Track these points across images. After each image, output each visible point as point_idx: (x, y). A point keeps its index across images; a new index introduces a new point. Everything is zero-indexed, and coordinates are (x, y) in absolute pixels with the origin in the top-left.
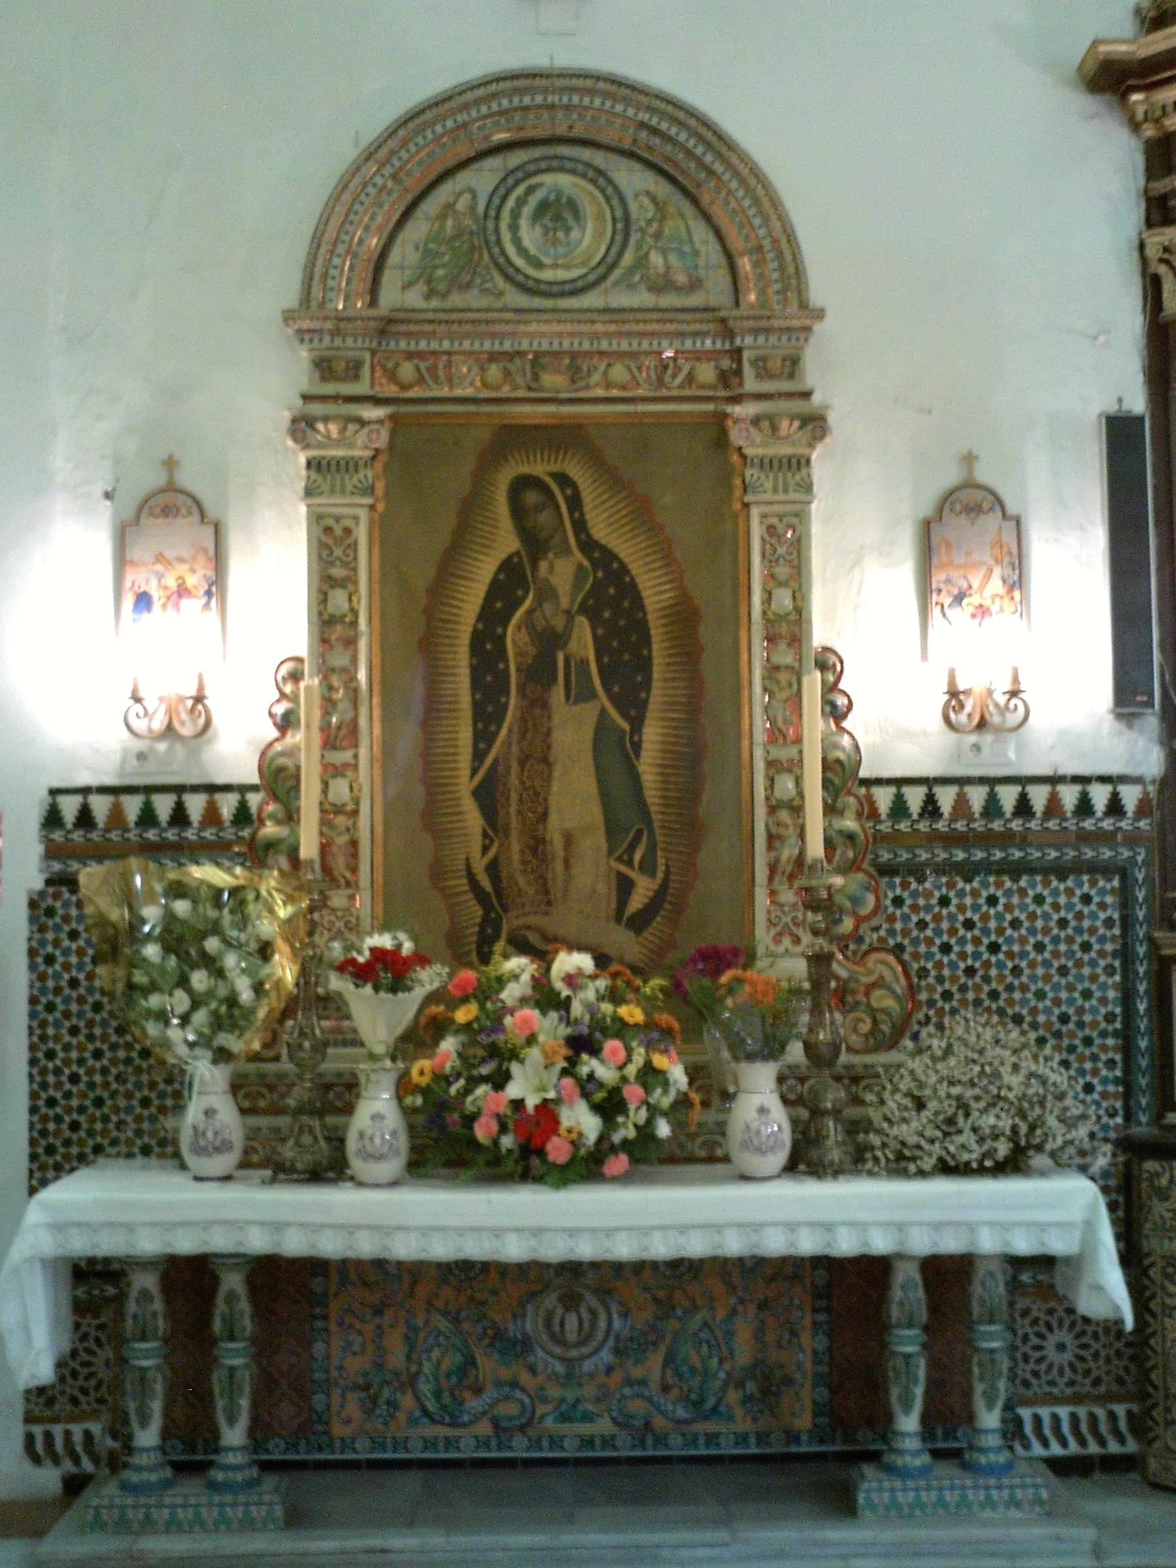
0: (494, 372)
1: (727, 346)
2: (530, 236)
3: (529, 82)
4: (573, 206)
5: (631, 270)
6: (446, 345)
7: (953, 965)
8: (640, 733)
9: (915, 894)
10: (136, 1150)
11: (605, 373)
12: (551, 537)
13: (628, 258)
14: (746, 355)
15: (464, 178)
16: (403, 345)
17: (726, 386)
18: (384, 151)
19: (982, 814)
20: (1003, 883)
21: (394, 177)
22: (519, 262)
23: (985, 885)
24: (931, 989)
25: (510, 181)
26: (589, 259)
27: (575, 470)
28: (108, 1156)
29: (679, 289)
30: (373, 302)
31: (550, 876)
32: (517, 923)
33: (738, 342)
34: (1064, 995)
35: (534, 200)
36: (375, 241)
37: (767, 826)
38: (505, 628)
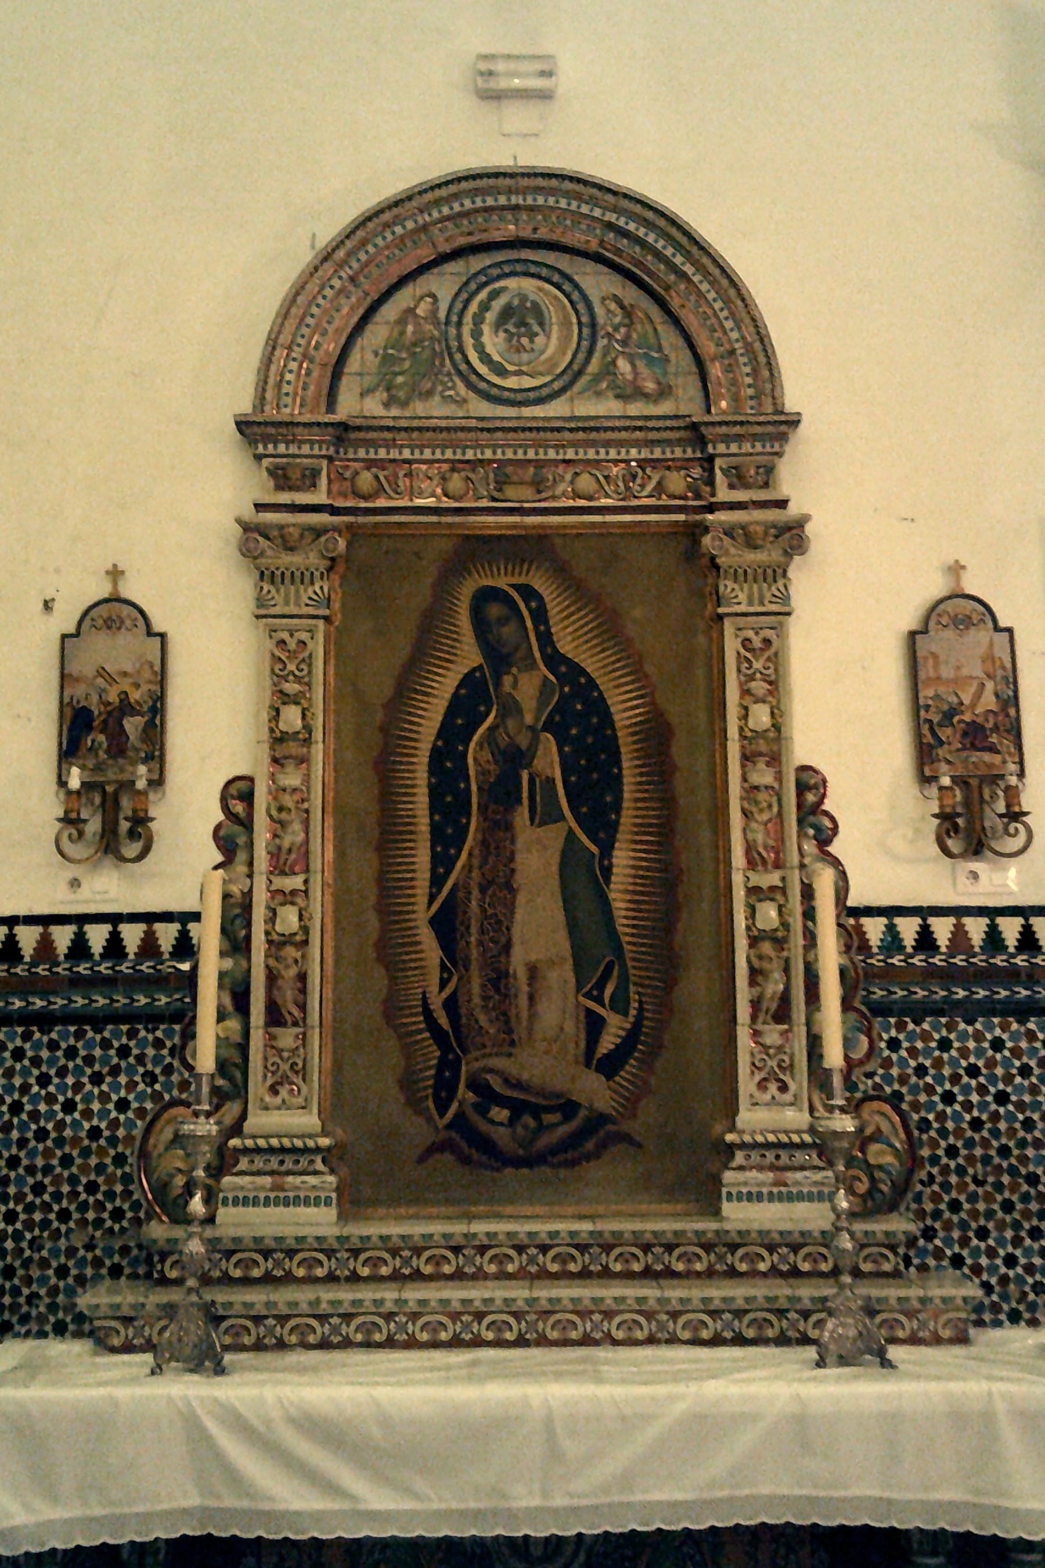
0: (456, 482)
1: (699, 455)
2: (494, 343)
3: (492, 182)
4: (537, 311)
5: (597, 379)
6: (406, 454)
7: (957, 1117)
8: (610, 856)
9: (911, 1037)
10: (48, 1328)
11: (572, 482)
12: (517, 648)
13: (593, 367)
14: (718, 462)
15: (430, 282)
16: (362, 453)
17: (698, 496)
18: (341, 253)
19: (66, 956)
20: (1010, 1024)
21: (352, 279)
22: (483, 369)
23: (117, 1034)
24: (934, 1144)
25: (473, 286)
26: (556, 365)
27: (539, 583)
28: (17, 1335)
29: (646, 396)
30: (331, 407)
31: (514, 1011)
32: (477, 1065)
33: (710, 449)
34: (93, 1161)
35: (498, 305)
36: (332, 346)
37: (749, 961)
38: (468, 745)
